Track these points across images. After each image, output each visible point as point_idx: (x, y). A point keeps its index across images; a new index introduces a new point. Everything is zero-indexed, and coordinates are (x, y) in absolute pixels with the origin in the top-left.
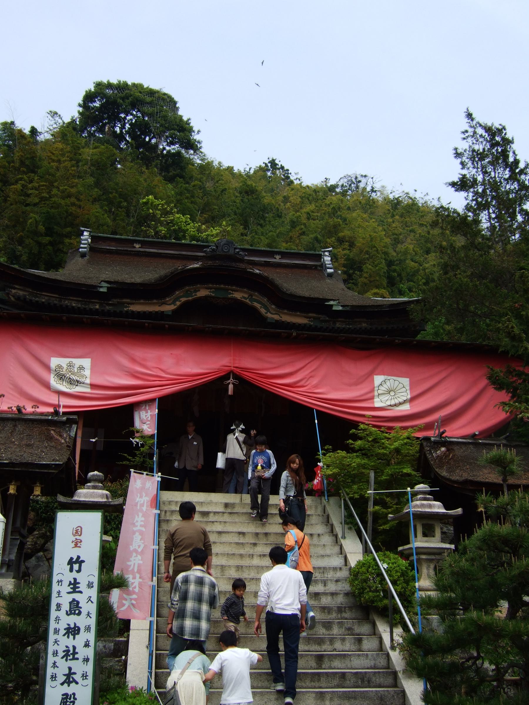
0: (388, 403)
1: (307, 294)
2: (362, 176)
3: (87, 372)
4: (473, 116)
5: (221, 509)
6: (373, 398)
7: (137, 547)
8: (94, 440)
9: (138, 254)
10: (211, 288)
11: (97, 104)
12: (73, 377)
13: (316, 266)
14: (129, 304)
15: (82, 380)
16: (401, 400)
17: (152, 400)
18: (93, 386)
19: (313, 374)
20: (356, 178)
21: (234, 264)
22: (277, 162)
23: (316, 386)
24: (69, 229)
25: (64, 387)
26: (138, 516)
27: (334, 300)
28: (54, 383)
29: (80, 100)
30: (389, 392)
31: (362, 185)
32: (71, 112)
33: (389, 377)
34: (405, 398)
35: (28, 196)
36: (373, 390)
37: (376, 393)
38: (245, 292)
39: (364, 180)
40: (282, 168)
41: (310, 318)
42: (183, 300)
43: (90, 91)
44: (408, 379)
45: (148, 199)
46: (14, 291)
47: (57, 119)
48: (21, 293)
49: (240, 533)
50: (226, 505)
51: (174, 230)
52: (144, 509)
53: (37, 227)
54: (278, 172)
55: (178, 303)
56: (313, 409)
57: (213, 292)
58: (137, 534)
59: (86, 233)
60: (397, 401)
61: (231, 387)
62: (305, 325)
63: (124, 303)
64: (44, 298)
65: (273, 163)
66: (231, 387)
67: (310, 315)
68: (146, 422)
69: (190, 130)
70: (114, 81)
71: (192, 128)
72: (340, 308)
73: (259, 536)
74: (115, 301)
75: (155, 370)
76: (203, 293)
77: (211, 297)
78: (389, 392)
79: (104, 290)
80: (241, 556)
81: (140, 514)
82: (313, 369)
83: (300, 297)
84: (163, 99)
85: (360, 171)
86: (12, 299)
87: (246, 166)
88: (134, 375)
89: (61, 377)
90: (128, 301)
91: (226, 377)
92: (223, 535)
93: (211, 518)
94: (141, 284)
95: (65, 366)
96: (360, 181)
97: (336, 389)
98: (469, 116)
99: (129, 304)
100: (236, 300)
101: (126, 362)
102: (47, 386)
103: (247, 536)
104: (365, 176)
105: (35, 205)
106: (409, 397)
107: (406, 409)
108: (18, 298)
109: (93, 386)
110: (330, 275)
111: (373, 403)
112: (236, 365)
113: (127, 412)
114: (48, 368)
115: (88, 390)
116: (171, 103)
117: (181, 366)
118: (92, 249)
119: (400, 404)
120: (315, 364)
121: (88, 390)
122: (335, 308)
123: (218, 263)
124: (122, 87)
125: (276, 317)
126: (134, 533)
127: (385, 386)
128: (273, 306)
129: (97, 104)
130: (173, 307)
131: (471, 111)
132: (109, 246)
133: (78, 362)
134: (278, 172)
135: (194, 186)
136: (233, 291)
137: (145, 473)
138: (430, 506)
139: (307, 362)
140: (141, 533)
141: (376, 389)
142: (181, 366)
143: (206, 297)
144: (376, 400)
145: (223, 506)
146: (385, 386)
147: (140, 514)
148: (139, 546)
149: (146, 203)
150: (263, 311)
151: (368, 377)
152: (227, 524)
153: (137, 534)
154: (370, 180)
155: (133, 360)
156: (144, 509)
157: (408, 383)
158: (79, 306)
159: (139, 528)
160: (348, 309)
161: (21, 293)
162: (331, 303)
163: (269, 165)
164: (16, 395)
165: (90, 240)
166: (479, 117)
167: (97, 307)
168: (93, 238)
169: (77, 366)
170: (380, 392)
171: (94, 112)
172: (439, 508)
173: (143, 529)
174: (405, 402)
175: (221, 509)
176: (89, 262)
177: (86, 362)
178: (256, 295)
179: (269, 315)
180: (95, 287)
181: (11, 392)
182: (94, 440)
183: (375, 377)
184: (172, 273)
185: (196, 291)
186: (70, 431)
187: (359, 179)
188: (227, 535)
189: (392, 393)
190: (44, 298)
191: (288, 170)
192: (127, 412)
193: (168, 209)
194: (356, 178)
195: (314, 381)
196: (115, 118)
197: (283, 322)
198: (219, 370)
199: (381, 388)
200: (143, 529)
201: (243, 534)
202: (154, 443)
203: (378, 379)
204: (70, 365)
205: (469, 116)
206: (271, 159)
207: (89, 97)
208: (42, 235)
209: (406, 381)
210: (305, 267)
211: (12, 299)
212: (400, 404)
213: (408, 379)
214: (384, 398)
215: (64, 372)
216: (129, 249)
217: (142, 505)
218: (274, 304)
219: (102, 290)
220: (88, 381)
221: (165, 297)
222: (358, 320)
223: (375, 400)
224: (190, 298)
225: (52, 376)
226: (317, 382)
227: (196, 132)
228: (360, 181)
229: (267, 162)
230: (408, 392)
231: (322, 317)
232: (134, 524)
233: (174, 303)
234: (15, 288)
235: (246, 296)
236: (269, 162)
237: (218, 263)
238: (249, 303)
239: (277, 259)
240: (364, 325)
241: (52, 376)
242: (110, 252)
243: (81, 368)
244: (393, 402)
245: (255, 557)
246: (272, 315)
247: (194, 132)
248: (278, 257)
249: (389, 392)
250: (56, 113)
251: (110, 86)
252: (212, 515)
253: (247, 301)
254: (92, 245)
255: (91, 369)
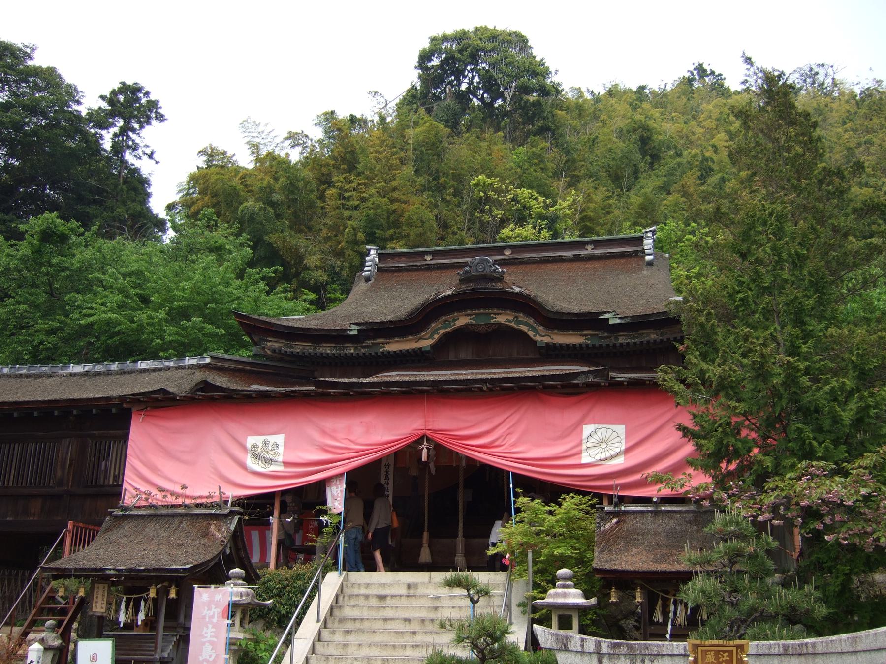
0: (598, 458)
1: (576, 310)
2: (818, 65)
3: (281, 450)
4: (753, 60)
5: (403, 591)
6: (580, 453)
7: (208, 657)
8: (289, 520)
9: (430, 268)
10: (471, 315)
11: (436, 62)
12: (267, 456)
13: (636, 252)
14: (384, 344)
15: (275, 458)
16: (613, 453)
17: (341, 475)
18: (286, 464)
19: (512, 429)
20: (811, 70)
21: (490, 285)
22: (705, 67)
23: (514, 445)
24: (391, 231)
25: (259, 467)
26: (207, 627)
27: (609, 313)
28: (251, 463)
29: (415, 60)
30: (602, 444)
31: (821, 77)
32: (409, 77)
33: (601, 426)
34: (618, 450)
35: (348, 199)
36: (580, 444)
37: (584, 447)
38: (508, 314)
39: (822, 72)
40: (713, 73)
41: (586, 335)
42: (441, 331)
43: (424, 50)
44: (623, 427)
45: (479, 180)
46: (269, 344)
47: (379, 98)
48: (276, 345)
49: (405, 620)
50: (409, 586)
51: (518, 209)
52: (215, 620)
53: (356, 235)
54: (707, 79)
55: (436, 337)
56: (508, 472)
57: (473, 319)
58: (207, 644)
59: (372, 252)
60: (608, 455)
61: (425, 452)
62: (581, 345)
63: (379, 344)
64: (299, 347)
65: (701, 70)
66: (425, 452)
67: (586, 332)
68: (336, 498)
69: (546, 73)
70: (449, 32)
71: (548, 68)
72: (618, 321)
73: (426, 623)
74: (369, 342)
75: (344, 441)
76: (462, 321)
77: (472, 325)
78: (600, 444)
79: (354, 333)
80: (394, 647)
81: (210, 626)
82: (512, 423)
83: (568, 314)
84: (509, 42)
85: (813, 61)
86: (269, 352)
87: (660, 83)
88: (324, 449)
89: (257, 457)
90: (382, 341)
91: (420, 440)
92: (389, 622)
93: (389, 602)
94: (391, 322)
95: (260, 445)
96: (817, 74)
97: (538, 445)
98: (748, 60)
99: (384, 344)
100: (500, 324)
101: (317, 436)
102: (244, 466)
103: (412, 623)
104: (823, 65)
105: (356, 208)
106: (623, 448)
107: (620, 463)
108: (274, 351)
109: (286, 464)
110: (650, 264)
111: (581, 458)
112: (430, 428)
113: (320, 487)
114: (244, 447)
115: (281, 468)
116: (521, 42)
117: (366, 435)
118: (380, 270)
119: (612, 457)
120: (516, 417)
121: (281, 468)
122: (611, 322)
123: (472, 286)
124: (460, 37)
125: (547, 340)
126: (204, 644)
127: (595, 436)
128: (541, 328)
129: (436, 62)
130: (430, 342)
131: (748, 55)
132: (398, 262)
133: (272, 439)
134: (707, 79)
135: (542, 149)
136: (495, 314)
137: (213, 586)
138: (565, 595)
139: (506, 416)
140: (212, 643)
141: (584, 441)
142: (366, 435)
143: (466, 325)
144: (584, 454)
145: (406, 587)
146: (595, 436)
147: (210, 626)
148: (210, 656)
149: (477, 185)
150: (531, 334)
151: (575, 429)
152: (399, 610)
153: (207, 644)
154: (830, 69)
155: (324, 433)
156: (215, 620)
157: (624, 430)
158: (334, 352)
159: (208, 639)
160: (627, 320)
161: (276, 345)
162: (606, 316)
163: (695, 72)
164: (216, 478)
165: (377, 260)
166: (759, 63)
167: (352, 351)
168: (380, 256)
169: (271, 443)
170: (589, 445)
171: (436, 70)
172: (575, 596)
173: (215, 639)
174: (618, 454)
175: (403, 591)
176: (370, 289)
177: (280, 439)
178: (522, 317)
179: (538, 338)
180: (345, 330)
181: (212, 476)
182: (289, 520)
183: (585, 427)
184: (423, 305)
185: (454, 320)
186: (231, 523)
187: (816, 70)
188: (393, 622)
189: (604, 445)
190: (299, 347)
191: (720, 75)
192: (320, 487)
193: (503, 187)
194: (811, 70)
195: (513, 439)
196: (459, 74)
197: (554, 344)
198: (411, 435)
199: (591, 439)
200: (215, 639)
201: (409, 620)
202: (340, 522)
203: (587, 429)
204: (265, 443)
205: (748, 60)
206: (696, 65)
207: (424, 58)
208: (363, 243)
209: (621, 429)
210: (622, 255)
211: (269, 352)
212: (612, 457)
213: (623, 427)
214: (592, 452)
215: (259, 450)
216: (419, 263)
217: (213, 617)
218: (542, 325)
219: (352, 333)
220: (281, 459)
221: (419, 332)
222: (643, 331)
223: (583, 455)
224: (449, 329)
225: (249, 455)
226: (511, 439)
227: (553, 73)
228: (817, 74)
229: (692, 69)
230: (623, 441)
231: (601, 333)
232: (203, 636)
233: (431, 337)
234: (270, 341)
235: (511, 318)
236: (695, 69)
237: (472, 286)
238: (515, 326)
239: (589, 250)
240: (653, 337)
241: (249, 455)
242: (398, 270)
243: (276, 445)
244: (603, 456)
245: (408, 648)
246: (542, 337)
247: (551, 73)
248: (590, 247)
249: (600, 444)
250: (376, 93)
251: (445, 39)
252: (389, 598)
253: (513, 324)
254: (381, 265)
255: (285, 446)
